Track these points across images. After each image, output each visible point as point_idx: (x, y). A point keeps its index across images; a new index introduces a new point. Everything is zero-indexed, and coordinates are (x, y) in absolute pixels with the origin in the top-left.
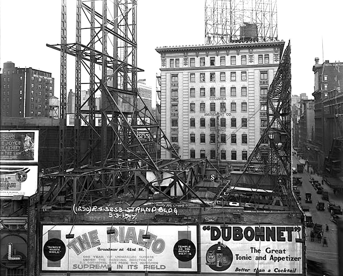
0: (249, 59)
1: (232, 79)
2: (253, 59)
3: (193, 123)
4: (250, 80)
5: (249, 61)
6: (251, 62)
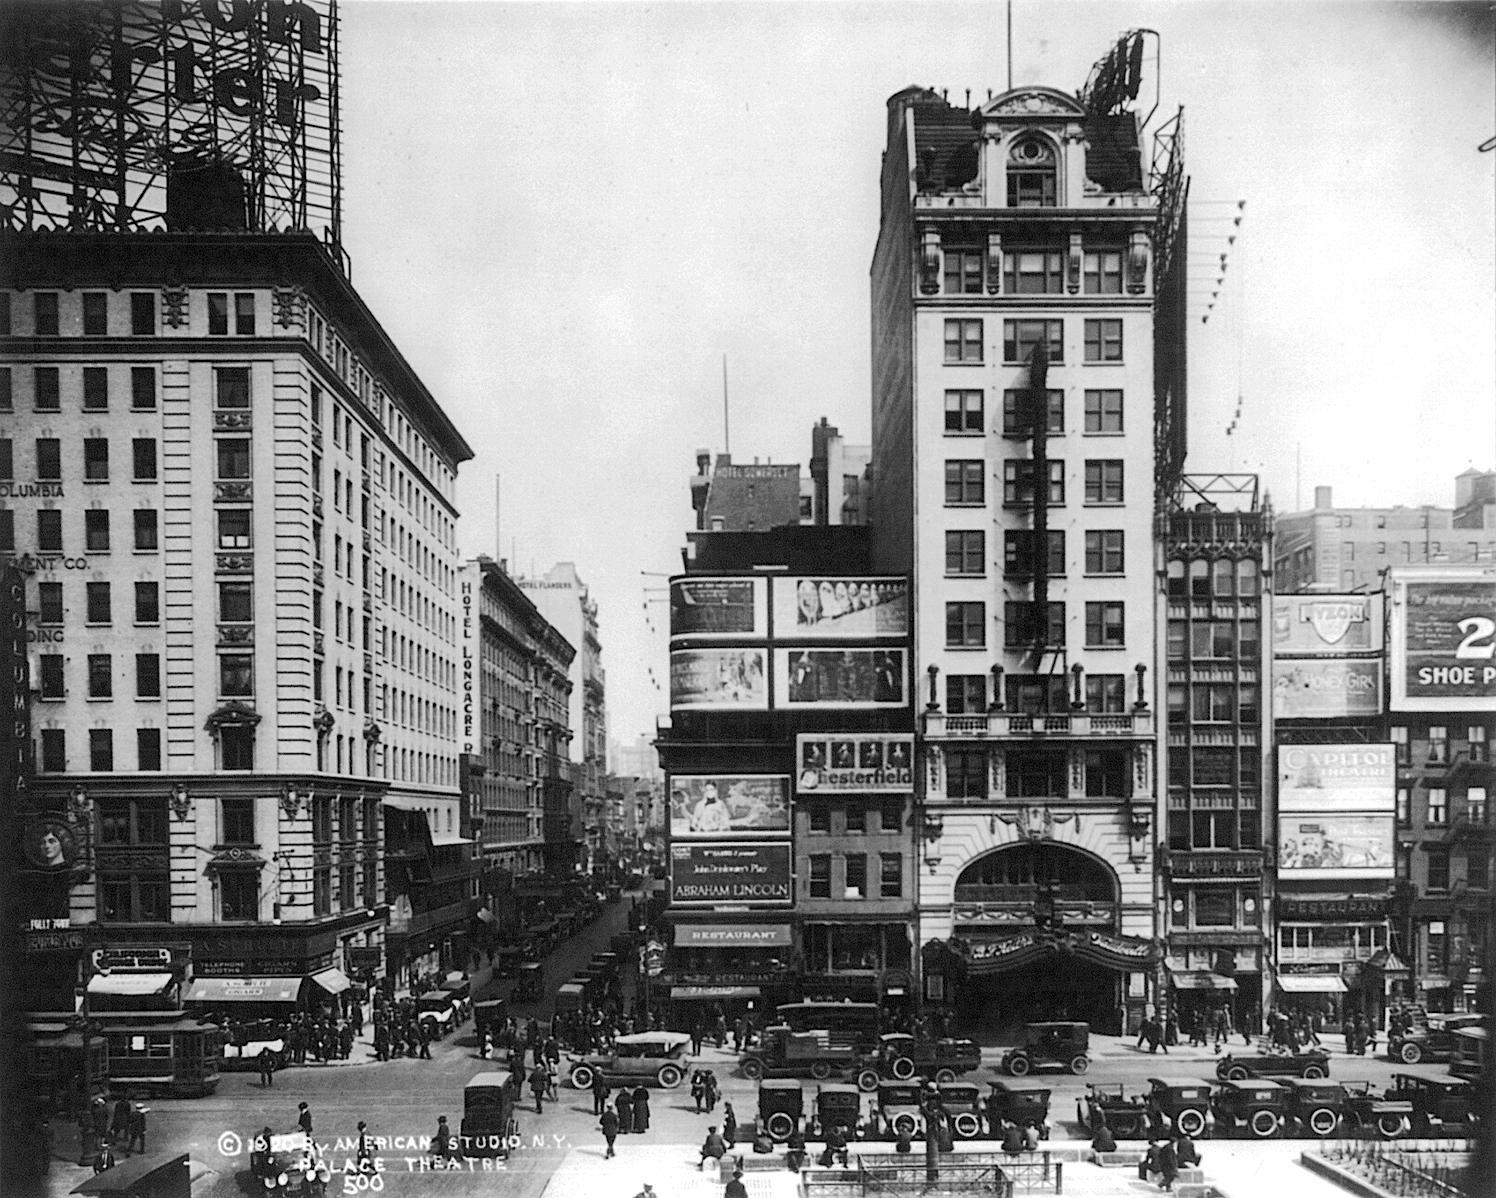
0: (166, 309)
1: (978, 398)
2: (184, 309)
3: (147, 606)
4: (171, 407)
5: (167, 318)
6: (175, 323)
